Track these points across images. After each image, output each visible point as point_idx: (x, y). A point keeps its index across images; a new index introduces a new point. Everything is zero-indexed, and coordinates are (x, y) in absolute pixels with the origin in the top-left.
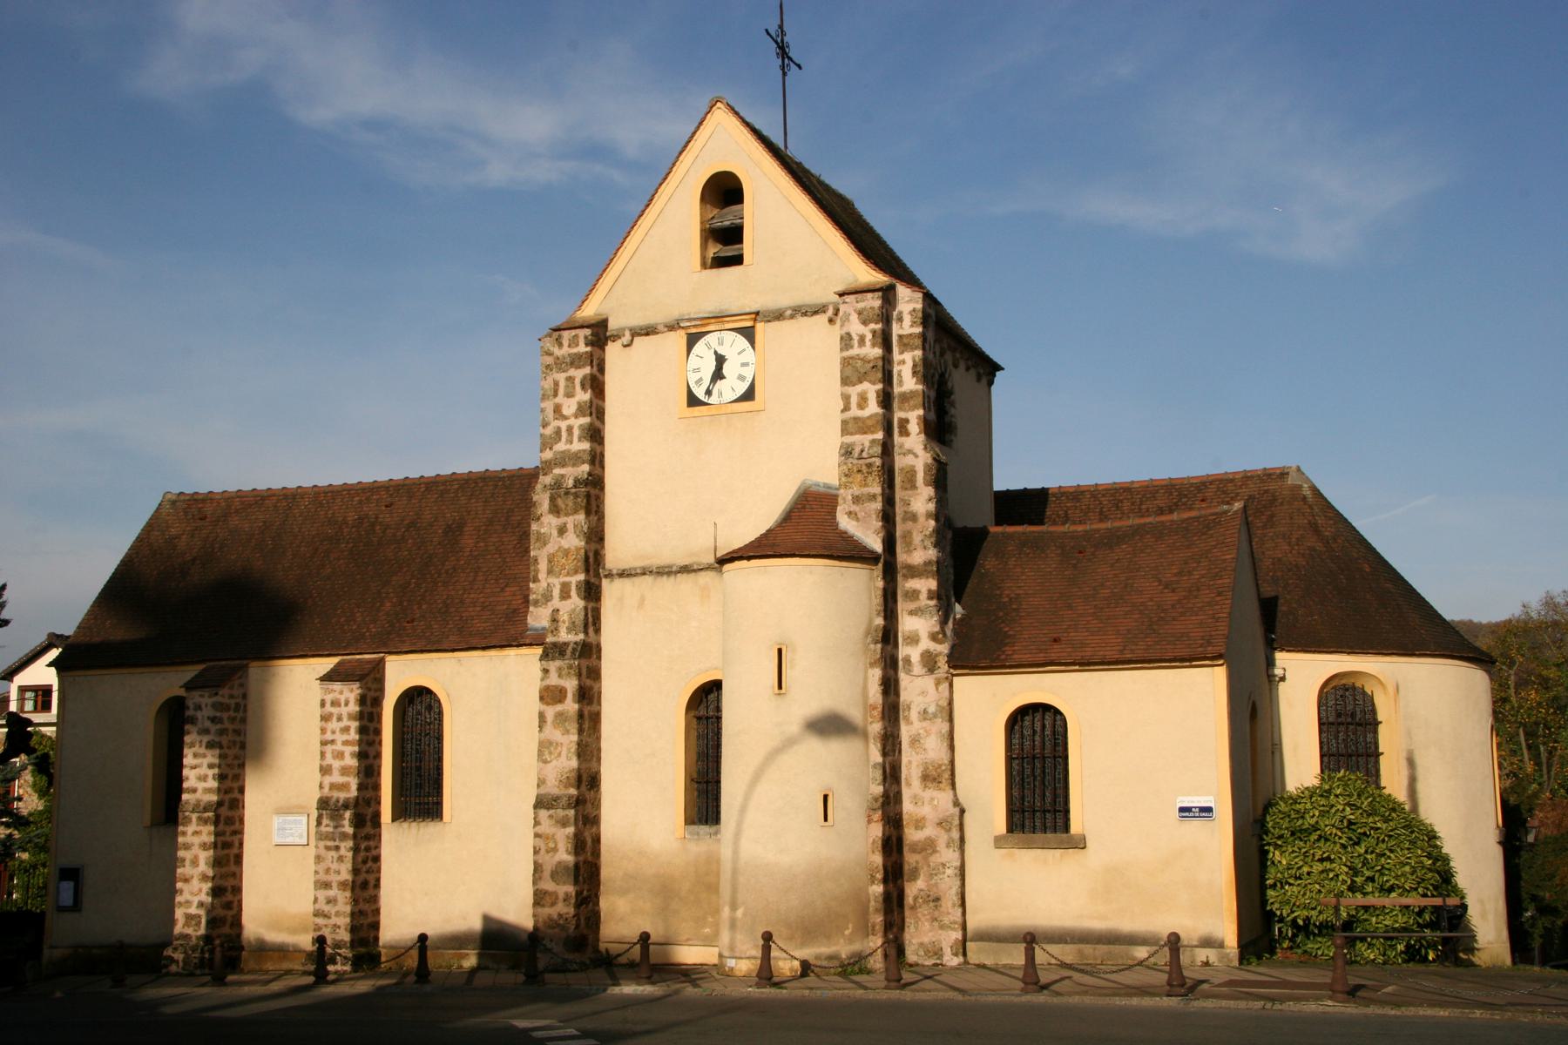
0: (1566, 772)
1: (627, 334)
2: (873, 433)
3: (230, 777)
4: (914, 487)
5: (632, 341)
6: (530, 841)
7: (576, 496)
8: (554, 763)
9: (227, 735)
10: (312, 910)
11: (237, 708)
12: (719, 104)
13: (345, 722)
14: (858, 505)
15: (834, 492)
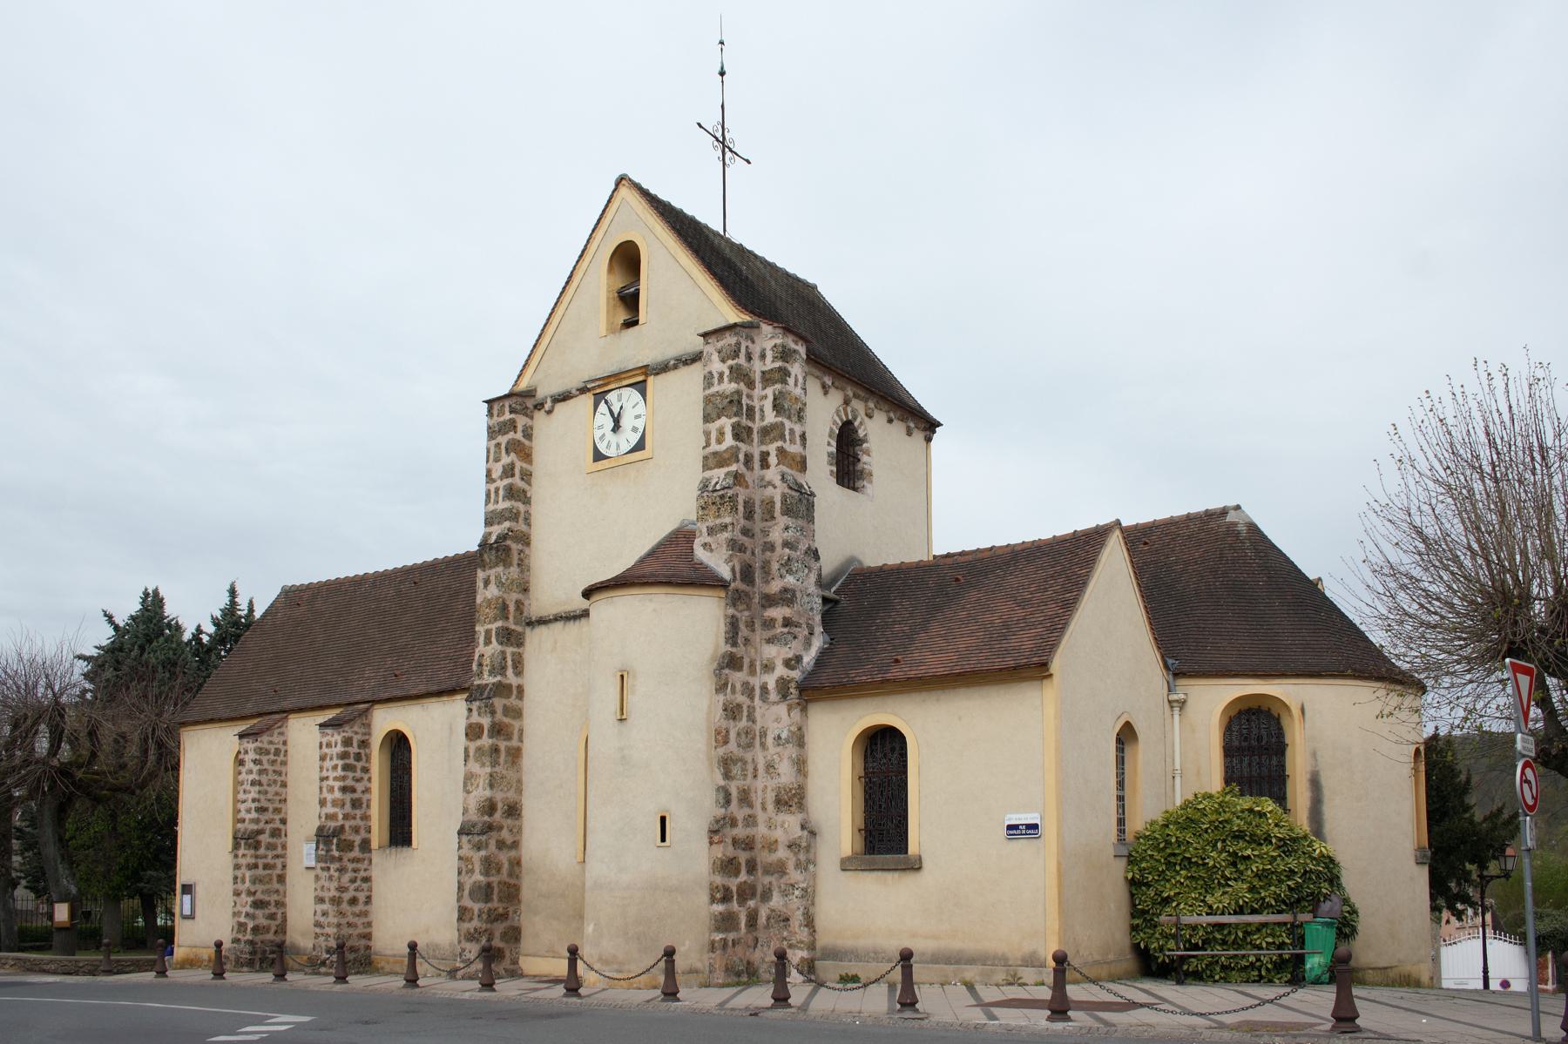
1: (549, 400)
2: (728, 465)
3: (271, 809)
4: (773, 518)
5: (553, 407)
6: (455, 862)
8: (475, 793)
9: (267, 775)
10: (313, 922)
11: (277, 752)
12: (623, 182)
13: (335, 761)
14: (712, 536)
15: (691, 527)
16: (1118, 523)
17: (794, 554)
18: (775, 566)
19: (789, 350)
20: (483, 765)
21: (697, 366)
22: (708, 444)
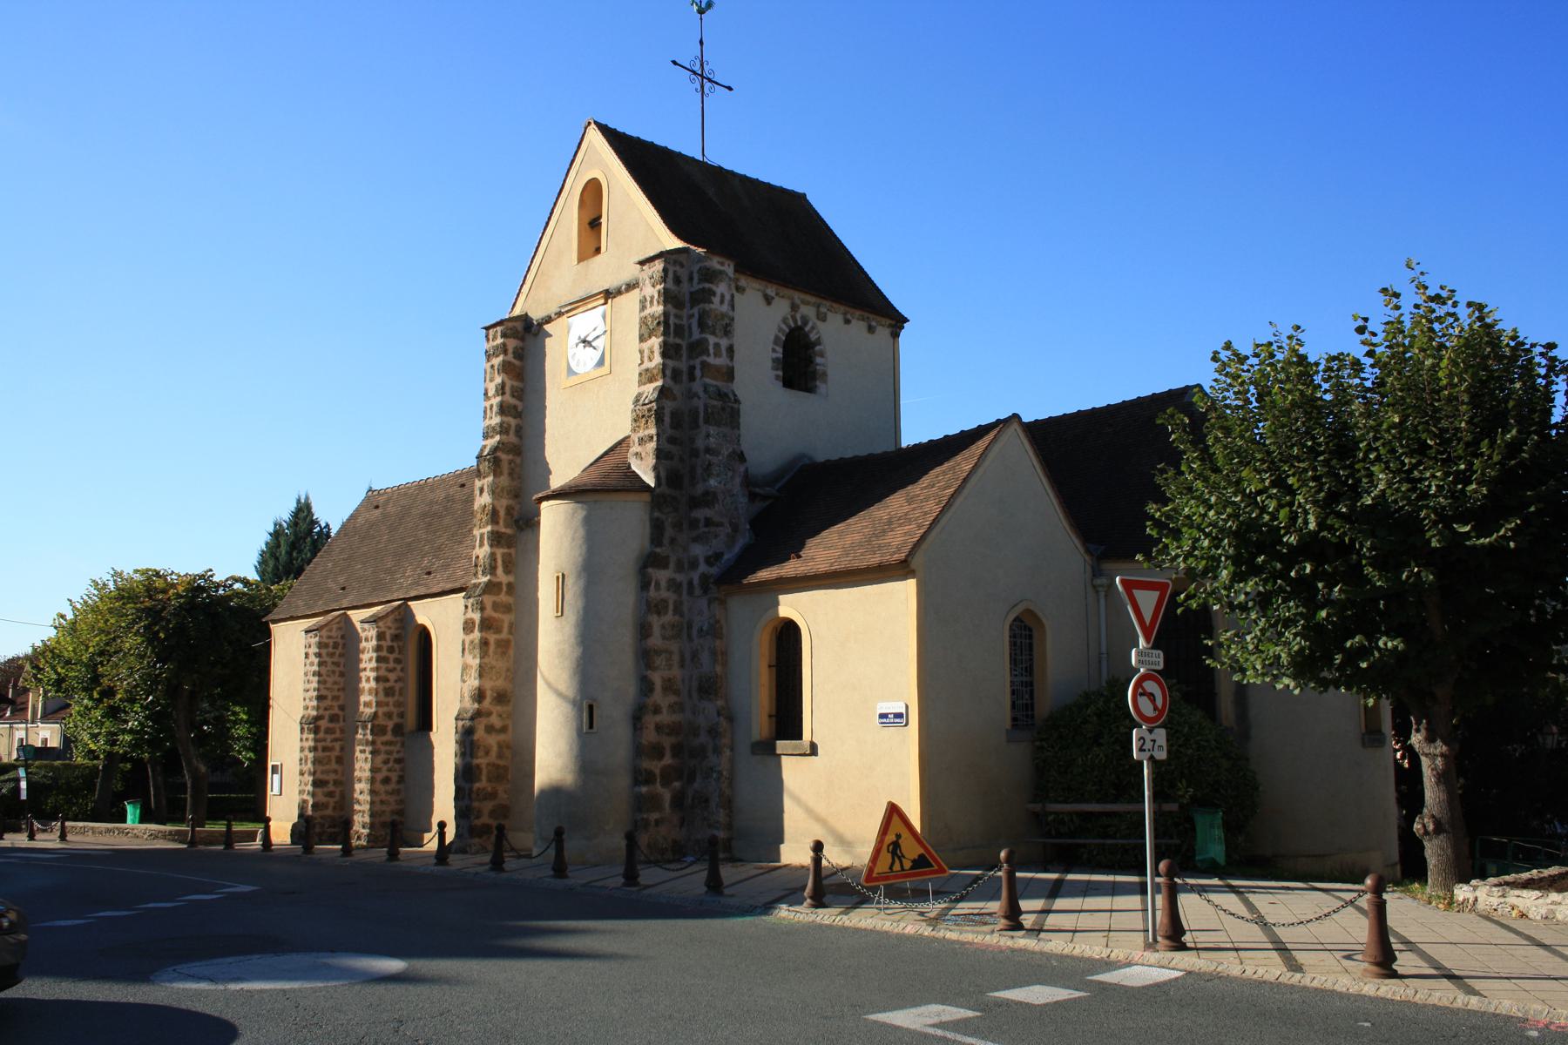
0: (1560, 668)
16: (1016, 416)
17: (714, 460)
18: (699, 471)
19: (714, 271)
20: (474, 657)
21: (637, 291)
22: (642, 362)
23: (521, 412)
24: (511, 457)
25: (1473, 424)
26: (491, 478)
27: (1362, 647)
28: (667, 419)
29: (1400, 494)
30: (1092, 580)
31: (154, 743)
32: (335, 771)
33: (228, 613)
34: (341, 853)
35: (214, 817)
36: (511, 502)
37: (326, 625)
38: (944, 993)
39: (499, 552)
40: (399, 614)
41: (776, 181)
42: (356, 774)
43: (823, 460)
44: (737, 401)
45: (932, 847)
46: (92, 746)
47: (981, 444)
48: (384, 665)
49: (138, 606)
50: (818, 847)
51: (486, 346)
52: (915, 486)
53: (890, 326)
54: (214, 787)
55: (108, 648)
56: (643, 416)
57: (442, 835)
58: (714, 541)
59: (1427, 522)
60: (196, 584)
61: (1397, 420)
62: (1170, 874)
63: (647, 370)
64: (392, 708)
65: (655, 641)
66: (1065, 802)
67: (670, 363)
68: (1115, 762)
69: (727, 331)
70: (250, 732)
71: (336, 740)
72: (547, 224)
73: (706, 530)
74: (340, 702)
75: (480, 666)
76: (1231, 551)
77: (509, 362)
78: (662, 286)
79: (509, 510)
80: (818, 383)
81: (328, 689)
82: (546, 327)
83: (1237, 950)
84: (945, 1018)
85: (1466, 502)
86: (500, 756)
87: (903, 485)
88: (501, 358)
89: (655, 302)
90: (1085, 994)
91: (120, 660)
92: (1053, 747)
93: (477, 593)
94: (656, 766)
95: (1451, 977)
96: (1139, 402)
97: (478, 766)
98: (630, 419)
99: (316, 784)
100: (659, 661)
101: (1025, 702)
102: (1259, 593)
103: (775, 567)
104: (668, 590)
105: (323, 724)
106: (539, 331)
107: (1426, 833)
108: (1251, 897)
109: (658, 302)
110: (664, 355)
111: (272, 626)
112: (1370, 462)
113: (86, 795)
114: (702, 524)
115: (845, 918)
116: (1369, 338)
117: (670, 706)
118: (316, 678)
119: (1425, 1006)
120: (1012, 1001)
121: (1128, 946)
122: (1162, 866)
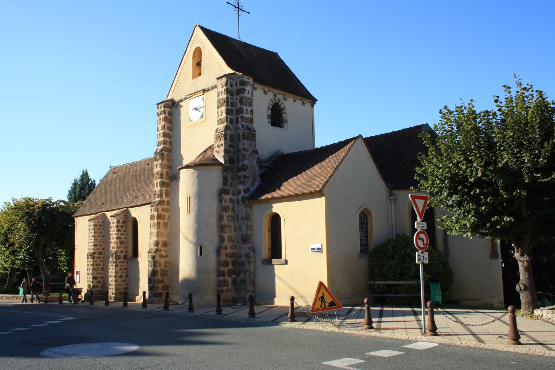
7: (159, 154)
16: (360, 136)
17: (246, 153)
18: (241, 157)
19: (245, 82)
20: (155, 229)
21: (216, 90)
23: (171, 136)
24: (167, 153)
25: (541, 136)
26: (160, 161)
27: (497, 220)
28: (228, 138)
29: (513, 163)
30: (389, 197)
31: (30, 264)
32: (101, 273)
33: (58, 214)
34: (105, 304)
35: (53, 291)
36: (168, 170)
37: (96, 218)
38: (349, 353)
39: (164, 189)
40: (125, 213)
41: (267, 48)
42: (109, 274)
43: (287, 153)
44: (255, 131)
45: (336, 297)
46: (6, 266)
47: (348, 146)
48: (119, 233)
49: (23, 211)
50: (292, 299)
51: (158, 111)
52: (323, 162)
53: (311, 102)
54: (53, 280)
55: (12, 228)
56: (219, 137)
57: (144, 297)
58: (247, 184)
59: (524, 173)
60: (45, 203)
61: (512, 135)
62: (432, 307)
63: (220, 119)
64: (122, 249)
65: (225, 222)
66: (381, 280)
67: (229, 117)
68: (399, 265)
69: (250, 105)
70: (66, 259)
71: (101, 261)
72: (180, 64)
73: (244, 180)
74: (103, 247)
75: (157, 233)
76: (448, 185)
77: (167, 117)
78: (226, 87)
79: (167, 173)
80: (284, 124)
81: (98, 242)
82: (181, 104)
83: (457, 335)
84: (352, 363)
85: (538, 165)
86: (165, 266)
87: (319, 162)
88: (163, 115)
89: (223, 94)
90: (403, 353)
91: (16, 232)
92: (376, 260)
93: (156, 205)
94: (226, 269)
95: (541, 344)
96: (410, 129)
97: (157, 270)
98: (214, 138)
99: (93, 278)
100: (227, 229)
101: (365, 243)
102: (458, 201)
103: (270, 194)
104: (229, 203)
105: (96, 255)
106: (178, 105)
107: (521, 290)
108: (456, 316)
109: (224, 93)
110: (227, 113)
111: (75, 218)
112: (501, 151)
113: (3, 284)
114: (242, 177)
115: (304, 325)
116: (499, 104)
117: (231, 247)
118: (93, 238)
119: (534, 355)
120: (376, 356)
121: (415, 334)
122: (428, 304)
